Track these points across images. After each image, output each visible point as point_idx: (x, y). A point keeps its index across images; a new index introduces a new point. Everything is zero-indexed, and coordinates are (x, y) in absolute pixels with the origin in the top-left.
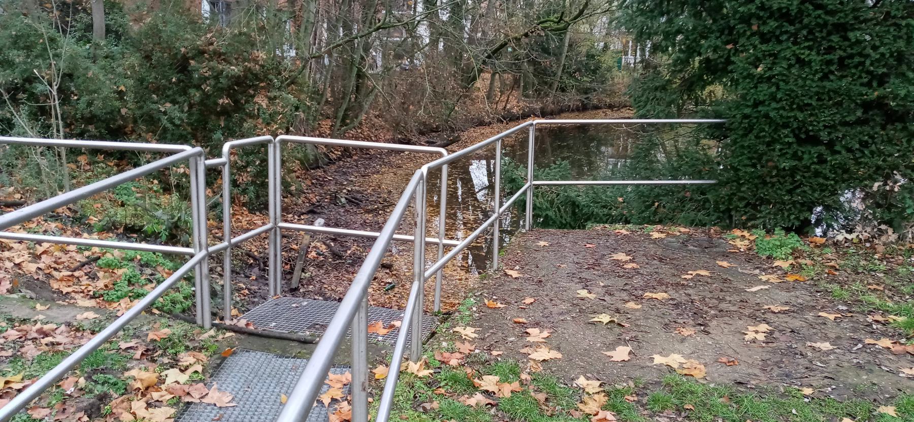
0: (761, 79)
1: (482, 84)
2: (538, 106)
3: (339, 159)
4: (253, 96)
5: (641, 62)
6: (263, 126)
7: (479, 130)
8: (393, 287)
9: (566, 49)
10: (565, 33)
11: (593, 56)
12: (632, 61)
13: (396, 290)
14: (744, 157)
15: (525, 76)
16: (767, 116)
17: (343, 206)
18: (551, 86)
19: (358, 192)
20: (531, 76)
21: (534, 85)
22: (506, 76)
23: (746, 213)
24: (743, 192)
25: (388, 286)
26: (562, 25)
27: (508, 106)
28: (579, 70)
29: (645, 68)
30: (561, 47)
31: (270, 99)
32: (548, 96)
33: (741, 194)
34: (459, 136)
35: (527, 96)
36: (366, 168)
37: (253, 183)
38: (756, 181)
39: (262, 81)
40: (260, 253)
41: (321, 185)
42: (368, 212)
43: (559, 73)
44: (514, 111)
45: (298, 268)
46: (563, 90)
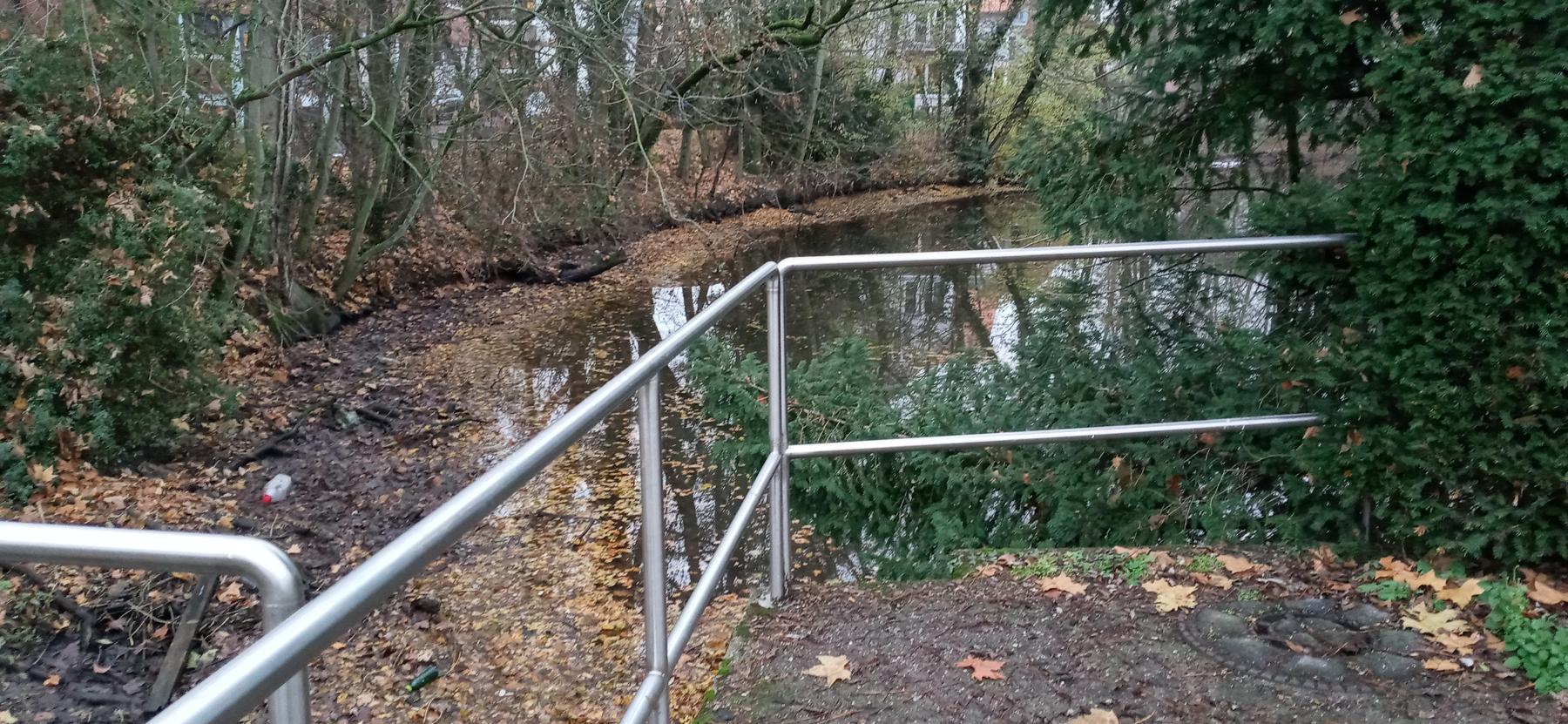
0: (1480, 112)
1: (668, 145)
2: (773, 187)
3: (366, 313)
4: (104, 195)
5: (952, 102)
6: (130, 263)
7: (666, 236)
8: (433, 678)
9: (819, 79)
10: (815, 53)
11: (867, 94)
12: (935, 103)
13: (442, 683)
14: (1422, 350)
15: (747, 134)
16: (1510, 227)
17: (351, 432)
18: (795, 150)
19: (394, 391)
20: (758, 132)
21: (763, 148)
22: (710, 134)
23: (1424, 514)
24: (1418, 454)
25: (421, 673)
26: (807, 34)
27: (719, 190)
28: (844, 119)
29: (957, 114)
30: (810, 75)
31: (146, 200)
32: (790, 168)
33: (1407, 460)
34: (622, 253)
35: (752, 170)
36: (424, 330)
37: (106, 402)
38: (1464, 423)
39: (124, 157)
40: (93, 596)
41: (311, 380)
42: (408, 442)
43: (809, 127)
44: (731, 197)
45: (181, 639)
46: (818, 157)
